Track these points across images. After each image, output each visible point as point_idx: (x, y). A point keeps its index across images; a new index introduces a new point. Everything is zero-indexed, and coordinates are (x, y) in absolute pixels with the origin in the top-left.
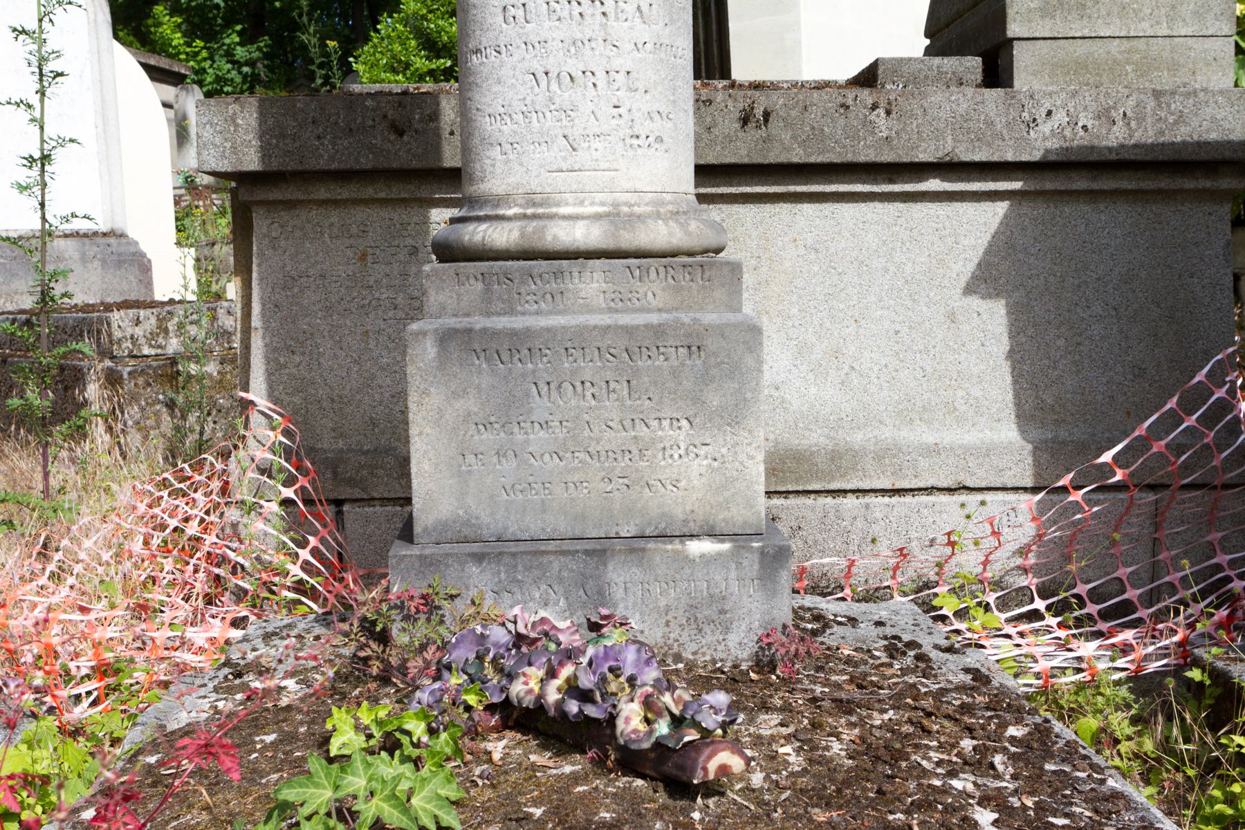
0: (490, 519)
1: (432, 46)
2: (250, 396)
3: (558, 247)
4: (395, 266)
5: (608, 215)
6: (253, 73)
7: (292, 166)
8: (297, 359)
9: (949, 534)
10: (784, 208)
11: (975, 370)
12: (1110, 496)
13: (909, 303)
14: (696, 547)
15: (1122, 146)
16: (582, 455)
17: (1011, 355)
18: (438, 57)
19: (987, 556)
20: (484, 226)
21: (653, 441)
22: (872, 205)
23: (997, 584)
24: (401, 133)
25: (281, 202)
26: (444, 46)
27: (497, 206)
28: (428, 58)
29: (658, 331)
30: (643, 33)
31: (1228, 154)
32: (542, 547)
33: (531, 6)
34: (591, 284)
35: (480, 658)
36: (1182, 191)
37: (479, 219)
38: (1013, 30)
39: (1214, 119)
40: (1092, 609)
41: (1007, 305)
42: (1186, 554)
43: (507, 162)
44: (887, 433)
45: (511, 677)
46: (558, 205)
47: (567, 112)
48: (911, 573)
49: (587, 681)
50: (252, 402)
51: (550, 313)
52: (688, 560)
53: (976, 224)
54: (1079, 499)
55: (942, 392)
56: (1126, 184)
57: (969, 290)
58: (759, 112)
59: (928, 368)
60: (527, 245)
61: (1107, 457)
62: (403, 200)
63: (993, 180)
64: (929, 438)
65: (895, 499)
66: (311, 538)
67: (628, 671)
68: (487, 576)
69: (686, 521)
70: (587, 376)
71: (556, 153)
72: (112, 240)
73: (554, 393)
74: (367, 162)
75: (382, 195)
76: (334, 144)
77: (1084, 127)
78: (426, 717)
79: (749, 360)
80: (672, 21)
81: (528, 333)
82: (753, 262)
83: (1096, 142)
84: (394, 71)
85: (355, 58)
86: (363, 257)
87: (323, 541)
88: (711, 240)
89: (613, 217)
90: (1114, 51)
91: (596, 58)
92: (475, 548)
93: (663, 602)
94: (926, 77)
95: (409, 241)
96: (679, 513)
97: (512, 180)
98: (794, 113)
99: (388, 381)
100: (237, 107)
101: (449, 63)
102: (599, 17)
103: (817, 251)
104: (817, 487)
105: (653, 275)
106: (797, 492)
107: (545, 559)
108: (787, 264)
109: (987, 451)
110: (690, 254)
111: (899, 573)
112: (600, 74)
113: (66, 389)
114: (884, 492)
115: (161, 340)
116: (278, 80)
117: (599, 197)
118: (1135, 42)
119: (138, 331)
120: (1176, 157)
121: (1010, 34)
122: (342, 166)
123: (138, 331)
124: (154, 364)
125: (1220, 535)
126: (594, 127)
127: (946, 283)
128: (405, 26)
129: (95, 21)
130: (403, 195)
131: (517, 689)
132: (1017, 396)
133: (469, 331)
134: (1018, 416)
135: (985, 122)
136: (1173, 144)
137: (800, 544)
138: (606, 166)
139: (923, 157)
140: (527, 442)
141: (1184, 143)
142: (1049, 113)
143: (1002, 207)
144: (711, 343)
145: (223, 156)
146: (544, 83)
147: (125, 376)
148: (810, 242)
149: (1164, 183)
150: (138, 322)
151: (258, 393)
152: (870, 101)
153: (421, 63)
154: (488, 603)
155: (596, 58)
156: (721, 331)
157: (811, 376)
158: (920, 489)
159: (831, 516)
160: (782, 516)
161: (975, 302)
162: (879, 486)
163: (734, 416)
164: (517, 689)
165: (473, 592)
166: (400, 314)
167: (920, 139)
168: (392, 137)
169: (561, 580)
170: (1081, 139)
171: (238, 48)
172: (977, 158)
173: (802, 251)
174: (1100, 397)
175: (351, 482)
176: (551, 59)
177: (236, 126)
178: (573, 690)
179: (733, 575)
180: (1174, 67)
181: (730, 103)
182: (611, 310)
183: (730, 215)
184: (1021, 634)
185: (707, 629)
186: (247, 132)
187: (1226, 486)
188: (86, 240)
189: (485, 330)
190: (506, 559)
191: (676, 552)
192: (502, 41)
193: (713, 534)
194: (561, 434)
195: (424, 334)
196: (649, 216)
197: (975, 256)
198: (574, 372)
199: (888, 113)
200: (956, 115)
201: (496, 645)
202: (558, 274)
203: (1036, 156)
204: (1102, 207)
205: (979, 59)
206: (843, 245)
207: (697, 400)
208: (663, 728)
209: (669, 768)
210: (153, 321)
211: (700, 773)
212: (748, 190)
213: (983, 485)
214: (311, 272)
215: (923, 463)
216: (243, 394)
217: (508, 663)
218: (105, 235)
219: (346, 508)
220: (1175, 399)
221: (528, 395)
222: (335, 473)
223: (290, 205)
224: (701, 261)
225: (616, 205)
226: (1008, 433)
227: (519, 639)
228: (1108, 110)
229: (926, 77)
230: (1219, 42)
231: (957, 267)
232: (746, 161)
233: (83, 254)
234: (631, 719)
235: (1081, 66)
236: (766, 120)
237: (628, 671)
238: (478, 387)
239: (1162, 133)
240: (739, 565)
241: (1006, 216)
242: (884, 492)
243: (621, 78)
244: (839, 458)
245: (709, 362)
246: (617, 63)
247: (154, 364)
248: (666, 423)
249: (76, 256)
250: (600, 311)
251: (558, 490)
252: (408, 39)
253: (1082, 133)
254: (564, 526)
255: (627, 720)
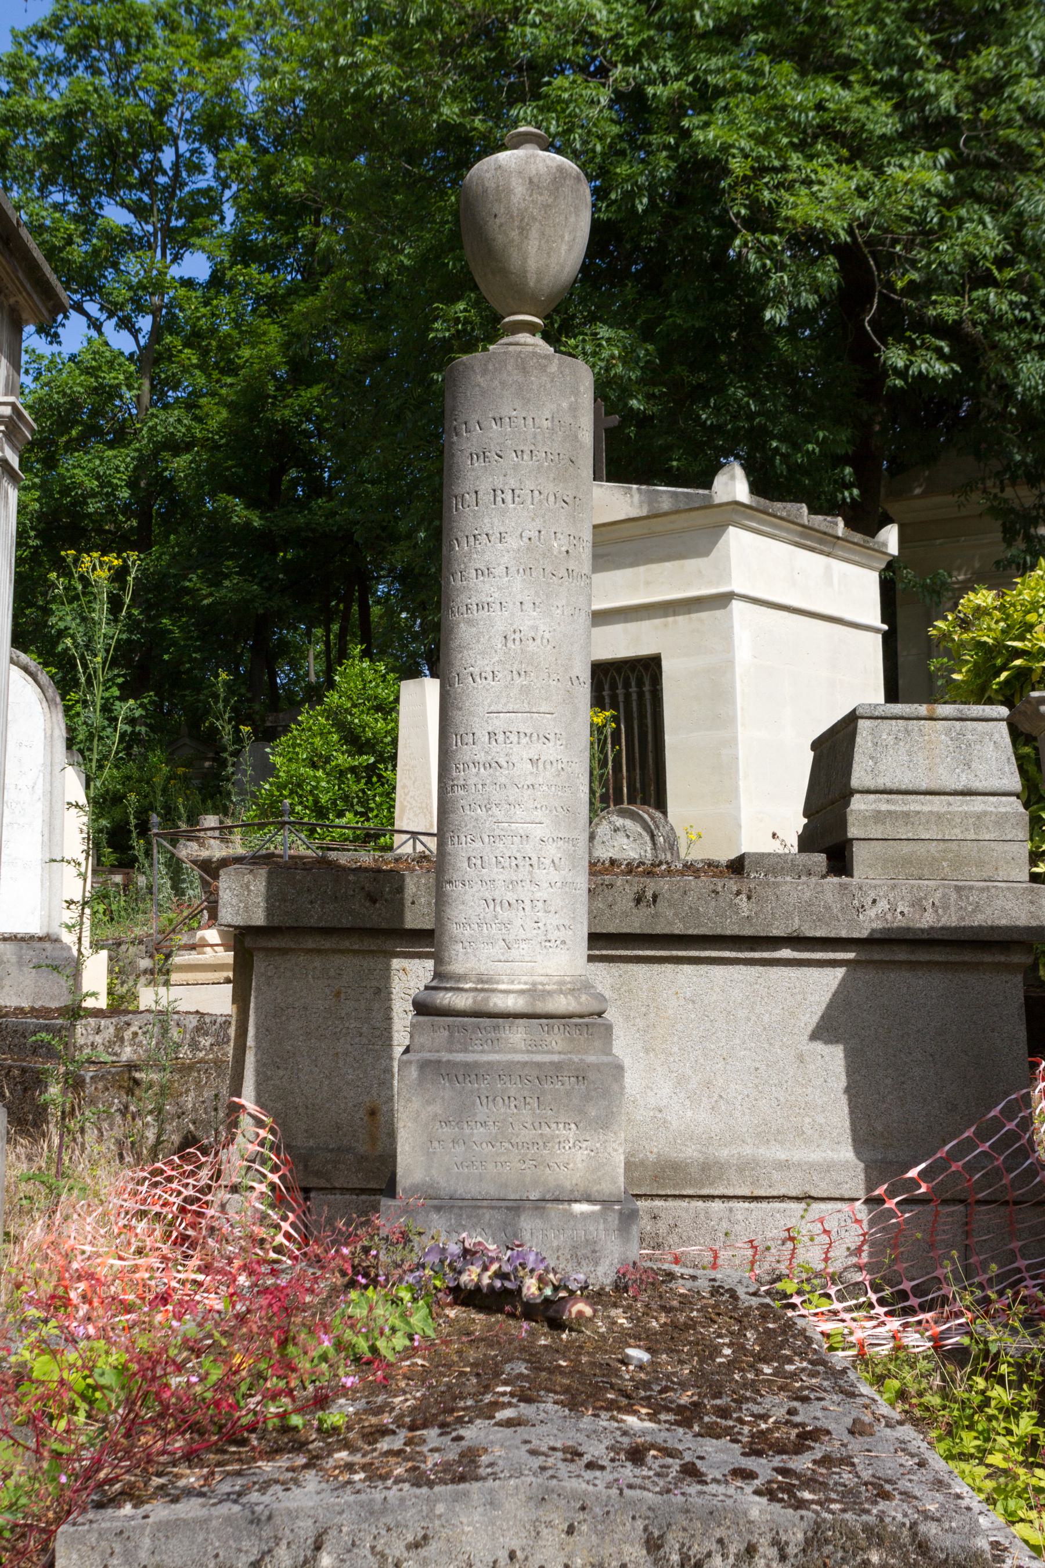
0: (446, 1184)
1: (355, 742)
2: (242, 1101)
3: (496, 1010)
4: (363, 1002)
5: (529, 990)
6: (133, 732)
7: (290, 923)
8: (281, 1073)
9: (788, 1230)
10: (669, 968)
11: (820, 1102)
12: (917, 1209)
13: (766, 1046)
14: (578, 1208)
15: (932, 928)
16: (507, 1145)
17: (848, 1090)
18: (361, 754)
19: (826, 1253)
20: (450, 994)
21: (553, 1137)
22: (737, 967)
23: (834, 1279)
24: (374, 901)
25: (278, 949)
26: (368, 740)
27: (458, 981)
28: (351, 754)
29: (558, 1066)
30: (555, 876)
31: (1015, 937)
32: (479, 1203)
33: (486, 858)
34: (517, 1035)
35: (442, 1262)
36: (982, 963)
37: (446, 989)
38: (853, 832)
39: (1003, 909)
40: (914, 1302)
41: (845, 1050)
42: (993, 1259)
43: (466, 953)
44: (748, 1150)
45: (460, 1273)
46: (497, 983)
47: (506, 924)
48: (766, 1266)
49: (507, 1268)
50: (243, 1106)
51: (490, 1052)
52: (572, 1215)
53: (819, 985)
54: (893, 1206)
55: (792, 1119)
56: (938, 957)
57: (814, 1036)
58: (649, 894)
59: (782, 1099)
60: (477, 1008)
61: (913, 1173)
62: (372, 952)
63: (833, 951)
64: (782, 1156)
65: (754, 1205)
66: (290, 1214)
67: (530, 1266)
68: (443, 1221)
69: (572, 1191)
70: (512, 1094)
71: (497, 950)
72: (47, 945)
73: (491, 1104)
74: (346, 922)
75: (356, 947)
76: (323, 908)
77: (902, 913)
78: (411, 1290)
79: (615, 1087)
80: (574, 867)
81: (476, 1065)
82: (644, 1009)
83: (911, 924)
84: (314, 766)
85: (273, 748)
86: (338, 994)
87: (298, 1217)
88: (596, 1007)
89: (533, 992)
90: (933, 850)
91: (524, 892)
92: (436, 1202)
93: (555, 1244)
94: (783, 868)
95: (375, 983)
96: (568, 1185)
97: (468, 965)
98: (676, 896)
99: (352, 1094)
100: (251, 877)
101: (372, 760)
102: (528, 867)
103: (694, 1002)
104: (690, 1192)
105: (556, 1030)
106: (675, 1196)
107: (480, 1212)
108: (670, 1012)
109: (828, 1167)
110: (581, 1016)
111: (756, 1266)
112: (527, 902)
113: (25, 1090)
114: (744, 1198)
115: (117, 1048)
116: (160, 741)
117: (524, 979)
118: (949, 844)
119: (98, 1039)
120: (975, 938)
121: (850, 835)
122: (328, 925)
123: (98, 1039)
124: (113, 1070)
125: (1020, 1243)
126: (522, 935)
127: (796, 1030)
128: (327, 719)
129: (52, 736)
130: (373, 948)
131: (464, 1278)
132: (853, 1123)
133: (439, 1062)
134: (854, 1140)
135: (825, 907)
136: (972, 927)
137: (676, 1239)
138: (528, 959)
139: (775, 933)
140: (472, 1134)
141: (980, 927)
142: (874, 901)
143: (840, 972)
144: (592, 1076)
145: (237, 914)
146: (492, 907)
147: (88, 1080)
148: (688, 995)
149: (968, 957)
150: (98, 1031)
151: (247, 1099)
152: (735, 889)
153: (342, 760)
154: (443, 1239)
155: (524, 892)
156: (598, 1067)
157: (687, 1102)
158: (774, 1197)
159: (702, 1216)
160: (662, 1215)
161: (819, 1046)
162: (740, 1193)
163: (605, 1123)
164: (464, 1278)
165: (433, 1232)
166: (365, 1041)
167: (774, 918)
168: (368, 904)
169: (490, 1225)
170: (899, 922)
171: (117, 703)
172: (818, 934)
173: (682, 1002)
174: (920, 1127)
175: (318, 1174)
176: (497, 892)
177: (250, 891)
178: (500, 1275)
179: (601, 1227)
180: (980, 864)
181: (627, 887)
182: (528, 1052)
183: (626, 972)
184: (854, 1320)
185: (583, 1263)
186: (257, 896)
187: (1016, 1203)
188: (23, 944)
189: (449, 1061)
190: (456, 1210)
191: (565, 1210)
192: (467, 878)
193: (589, 1200)
194: (494, 1130)
195: (411, 1062)
196: (555, 992)
197: (819, 1010)
198: (504, 1091)
199: (749, 898)
200: (812, 900)
201: (452, 1255)
202: (496, 1028)
203: (865, 934)
204: (920, 974)
205: (824, 856)
206: (714, 998)
207: (581, 1112)
208: (548, 1291)
209: (551, 1313)
210: (112, 1030)
211: (567, 1313)
212: (640, 953)
213: (825, 1195)
214: (297, 1005)
215: (776, 1176)
216: (236, 1099)
217: (458, 1265)
218: (40, 939)
219: (312, 1195)
220: (973, 1129)
221: (474, 1104)
222: (306, 1166)
223: (284, 952)
224: (589, 1022)
225: (534, 984)
226: (846, 1153)
227: (466, 1252)
228: (920, 900)
229: (783, 868)
230: (1016, 846)
231: (804, 1019)
232: (638, 931)
233: (21, 957)
234: (531, 1288)
235: (907, 861)
236: (655, 901)
237: (530, 1266)
238: (443, 1098)
239: (963, 919)
240: (605, 1221)
241: (843, 979)
242: (744, 1198)
243: (540, 904)
244: (710, 1169)
245: (587, 1085)
246: (538, 895)
247: (113, 1070)
248: (561, 1126)
249: (14, 959)
250: (522, 1052)
251: (491, 1167)
252: (330, 733)
253: (900, 917)
254: (493, 1191)
255: (529, 1288)
